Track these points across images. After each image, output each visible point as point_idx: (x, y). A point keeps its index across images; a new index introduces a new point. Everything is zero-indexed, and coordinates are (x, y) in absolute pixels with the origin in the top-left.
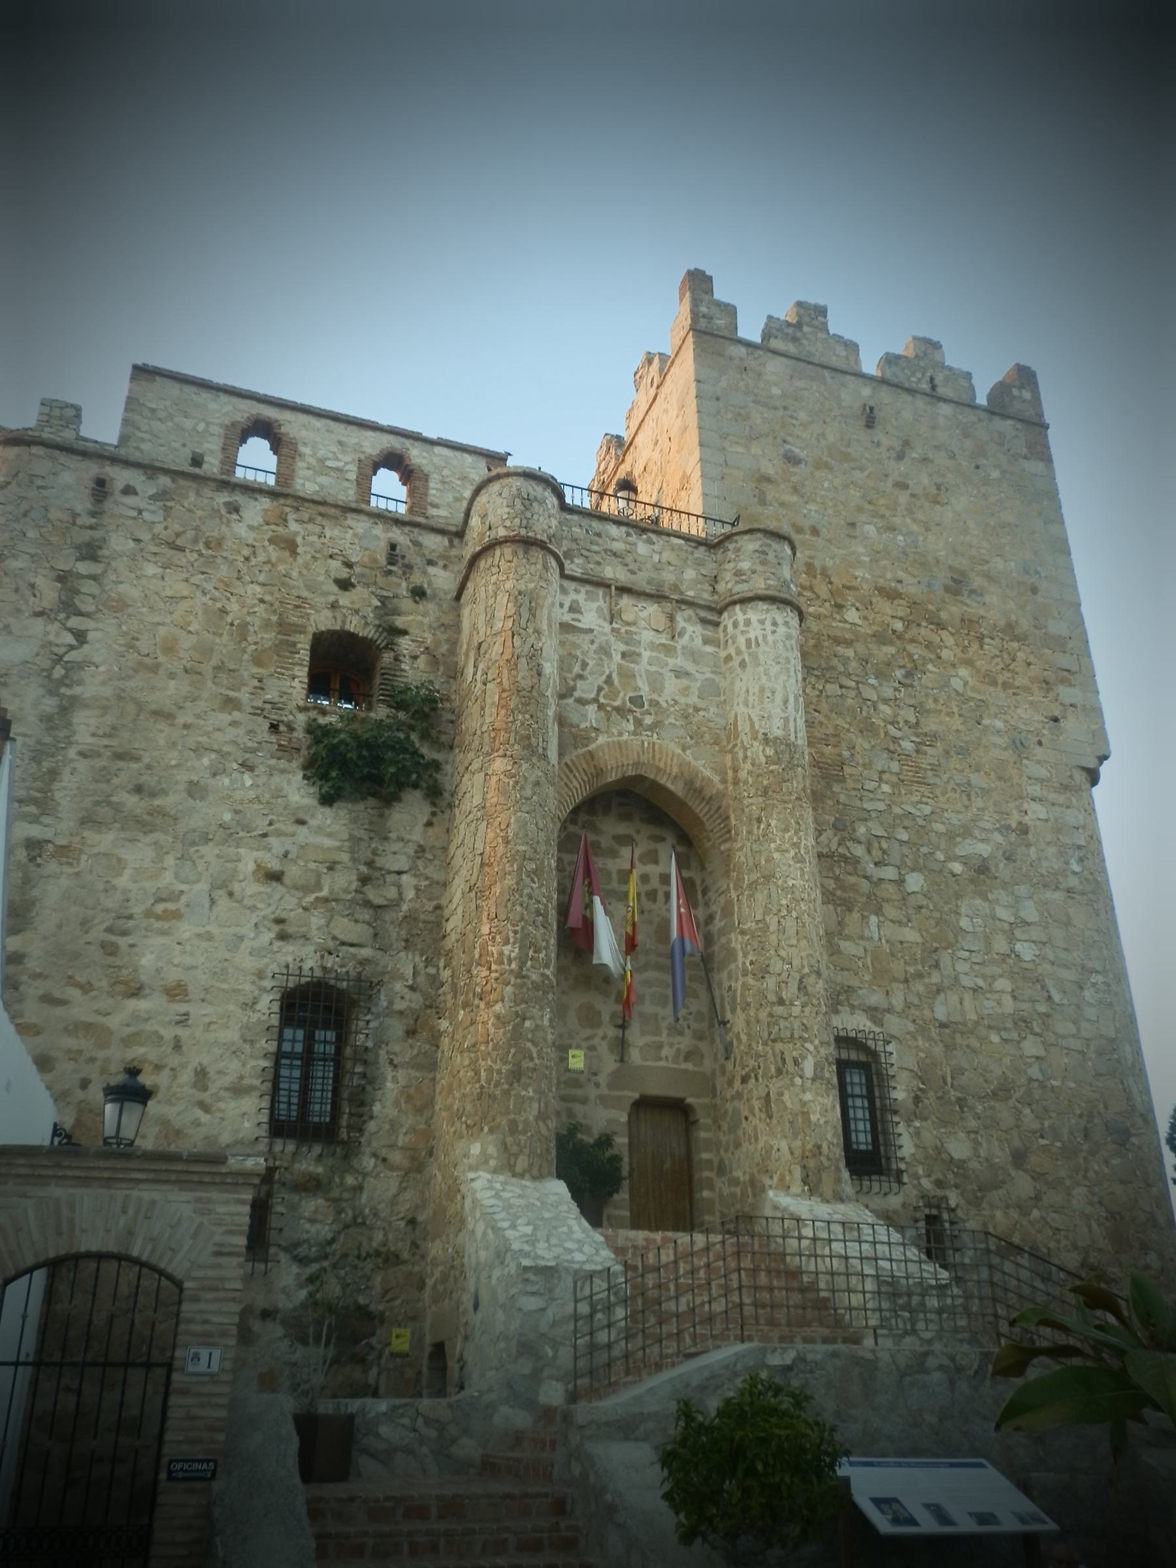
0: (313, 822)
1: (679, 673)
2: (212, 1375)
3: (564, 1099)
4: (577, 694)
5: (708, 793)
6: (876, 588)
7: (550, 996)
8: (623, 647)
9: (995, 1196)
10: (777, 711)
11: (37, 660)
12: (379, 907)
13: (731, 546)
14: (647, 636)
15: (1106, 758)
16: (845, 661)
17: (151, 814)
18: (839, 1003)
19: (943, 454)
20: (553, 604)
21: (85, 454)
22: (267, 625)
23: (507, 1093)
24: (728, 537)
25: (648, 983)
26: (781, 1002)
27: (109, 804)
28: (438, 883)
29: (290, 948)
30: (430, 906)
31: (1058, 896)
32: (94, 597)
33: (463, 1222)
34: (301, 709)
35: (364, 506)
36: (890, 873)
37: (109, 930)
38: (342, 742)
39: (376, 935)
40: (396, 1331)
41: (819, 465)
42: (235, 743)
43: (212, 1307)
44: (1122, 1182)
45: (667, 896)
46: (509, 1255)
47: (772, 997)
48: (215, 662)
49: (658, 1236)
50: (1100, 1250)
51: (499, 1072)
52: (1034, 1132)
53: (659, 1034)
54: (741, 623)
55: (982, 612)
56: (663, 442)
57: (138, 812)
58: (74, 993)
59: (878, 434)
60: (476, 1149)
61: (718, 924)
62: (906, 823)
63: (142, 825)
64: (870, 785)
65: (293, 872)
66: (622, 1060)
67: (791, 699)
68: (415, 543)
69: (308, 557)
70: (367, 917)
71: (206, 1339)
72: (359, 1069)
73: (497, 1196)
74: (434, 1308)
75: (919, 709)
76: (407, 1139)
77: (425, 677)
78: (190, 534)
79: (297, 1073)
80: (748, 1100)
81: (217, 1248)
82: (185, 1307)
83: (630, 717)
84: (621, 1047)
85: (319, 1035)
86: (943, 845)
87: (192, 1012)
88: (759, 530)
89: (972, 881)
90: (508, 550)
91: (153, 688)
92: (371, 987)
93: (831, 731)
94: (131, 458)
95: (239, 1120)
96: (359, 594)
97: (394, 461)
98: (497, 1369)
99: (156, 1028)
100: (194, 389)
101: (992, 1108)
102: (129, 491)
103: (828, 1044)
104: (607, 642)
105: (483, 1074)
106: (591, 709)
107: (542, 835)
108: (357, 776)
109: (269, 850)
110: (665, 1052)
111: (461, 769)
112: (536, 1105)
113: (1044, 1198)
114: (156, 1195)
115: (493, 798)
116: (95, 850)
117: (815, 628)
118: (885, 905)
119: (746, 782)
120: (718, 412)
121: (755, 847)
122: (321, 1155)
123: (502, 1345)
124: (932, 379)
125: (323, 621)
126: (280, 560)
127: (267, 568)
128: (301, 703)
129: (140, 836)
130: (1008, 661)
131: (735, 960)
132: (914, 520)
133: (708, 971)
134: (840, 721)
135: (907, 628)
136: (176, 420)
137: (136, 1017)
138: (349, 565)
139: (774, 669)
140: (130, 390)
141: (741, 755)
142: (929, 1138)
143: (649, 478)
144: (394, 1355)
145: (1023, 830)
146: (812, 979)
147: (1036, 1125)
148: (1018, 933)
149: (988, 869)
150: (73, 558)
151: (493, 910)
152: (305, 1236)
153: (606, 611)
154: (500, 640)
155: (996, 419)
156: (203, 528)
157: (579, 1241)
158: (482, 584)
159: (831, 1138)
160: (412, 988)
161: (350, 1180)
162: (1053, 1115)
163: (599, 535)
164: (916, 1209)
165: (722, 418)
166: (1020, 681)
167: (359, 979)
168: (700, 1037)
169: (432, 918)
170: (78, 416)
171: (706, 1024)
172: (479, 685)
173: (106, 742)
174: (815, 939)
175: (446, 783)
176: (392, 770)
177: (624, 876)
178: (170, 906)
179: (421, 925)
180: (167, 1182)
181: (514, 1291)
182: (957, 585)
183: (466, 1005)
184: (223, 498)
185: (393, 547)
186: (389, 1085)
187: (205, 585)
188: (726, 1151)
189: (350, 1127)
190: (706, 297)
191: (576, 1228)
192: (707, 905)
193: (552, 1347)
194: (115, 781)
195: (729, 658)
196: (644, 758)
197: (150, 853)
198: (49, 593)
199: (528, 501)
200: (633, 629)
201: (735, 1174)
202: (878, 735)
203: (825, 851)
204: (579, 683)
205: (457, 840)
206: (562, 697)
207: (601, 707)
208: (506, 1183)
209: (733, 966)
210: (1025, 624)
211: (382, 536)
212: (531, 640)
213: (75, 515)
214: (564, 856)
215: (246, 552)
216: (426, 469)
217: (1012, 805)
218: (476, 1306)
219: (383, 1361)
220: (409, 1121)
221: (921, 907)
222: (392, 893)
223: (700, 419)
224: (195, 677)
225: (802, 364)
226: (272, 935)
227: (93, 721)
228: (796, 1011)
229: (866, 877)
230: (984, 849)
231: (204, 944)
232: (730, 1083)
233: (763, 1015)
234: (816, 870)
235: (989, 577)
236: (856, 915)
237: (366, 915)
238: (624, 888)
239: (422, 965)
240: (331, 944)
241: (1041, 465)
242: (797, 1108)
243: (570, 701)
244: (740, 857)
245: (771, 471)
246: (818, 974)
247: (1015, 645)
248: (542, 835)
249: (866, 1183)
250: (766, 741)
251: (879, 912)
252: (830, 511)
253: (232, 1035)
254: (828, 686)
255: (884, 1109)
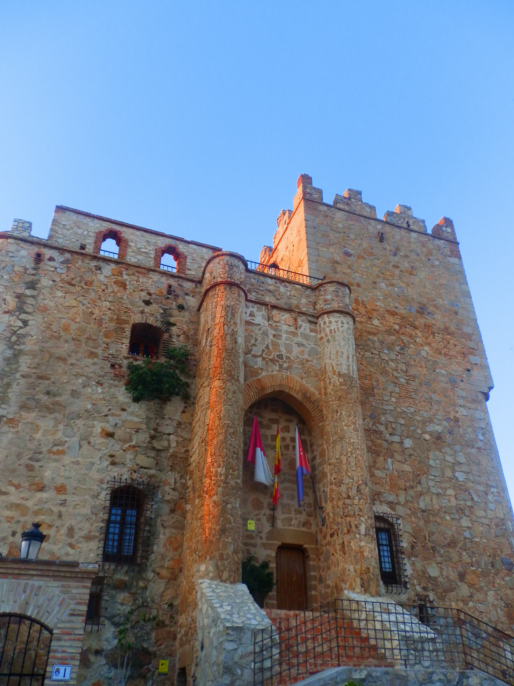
0: (129, 410)
1: (299, 345)
2: (66, 681)
3: (245, 544)
4: (253, 353)
5: (313, 399)
6: (386, 310)
7: (240, 493)
8: (274, 332)
9: (452, 595)
10: (344, 362)
11: (5, 333)
12: (159, 450)
13: (322, 289)
14: (285, 328)
15: (492, 388)
16: (373, 342)
17: (54, 405)
18: (374, 500)
19: (414, 254)
20: (242, 312)
21: (32, 243)
22: (111, 320)
23: (218, 540)
24: (321, 285)
25: (285, 489)
26: (349, 497)
27: (34, 399)
28: (187, 439)
29: (117, 469)
30: (183, 450)
31: (474, 451)
32: (33, 305)
33: (196, 605)
34: (126, 358)
35: (157, 269)
36: (396, 439)
37: (31, 459)
38: (144, 372)
39: (157, 463)
40: (161, 661)
41: (360, 257)
42: (94, 372)
43: (68, 643)
44: (511, 589)
45: (294, 447)
46: (219, 621)
47: (344, 495)
48: (86, 336)
49: (291, 613)
50: (502, 623)
51: (215, 529)
52: (468, 564)
53: (291, 514)
54: (327, 322)
55: (433, 322)
56: (290, 247)
57: (47, 403)
58: (12, 489)
59: (385, 245)
60: (203, 568)
61: (318, 461)
62: (403, 416)
63: (49, 410)
64: (386, 398)
65: (119, 433)
66: (273, 526)
67: (351, 357)
68: (180, 285)
69: (131, 290)
70: (153, 455)
71: (63, 662)
72: (147, 528)
73: (213, 591)
74: (181, 650)
75: (407, 364)
76: (170, 563)
77: (183, 344)
78: (78, 279)
79: (117, 531)
80: (334, 545)
81: (71, 612)
82: (53, 643)
83: (277, 364)
84: (273, 519)
85: (129, 512)
86: (420, 426)
87: (68, 499)
88: (335, 282)
89: (434, 443)
90: (222, 288)
91: (58, 347)
92: (154, 489)
93: (368, 373)
94: (53, 245)
95: (88, 554)
96: (154, 307)
97: (171, 250)
98: (212, 681)
99: (51, 506)
100: (83, 217)
101: (448, 551)
102: (51, 259)
103: (371, 518)
104: (266, 330)
105: (207, 530)
106: (259, 359)
107: (236, 416)
108: (151, 388)
109: (108, 422)
110: (294, 522)
111: (199, 386)
112: (232, 546)
113: (475, 596)
114: (41, 583)
115: (213, 398)
116: (26, 421)
117: (359, 328)
118: (395, 453)
119: (330, 394)
120: (315, 233)
121: (335, 424)
122: (127, 571)
123: (215, 668)
124: (408, 222)
125: (137, 319)
126: (118, 291)
127: (112, 294)
128: (126, 355)
129: (48, 415)
130: (446, 344)
131: (327, 477)
132: (402, 281)
133: (313, 483)
134: (371, 369)
135: (400, 328)
136: (74, 229)
137: (41, 501)
138: (149, 294)
139: (343, 343)
140: (54, 216)
141: (328, 381)
142: (419, 566)
143: (284, 263)
144: (160, 674)
145: (457, 420)
146: (363, 487)
147: (469, 560)
148: (456, 468)
149: (441, 438)
150: (24, 288)
151: (213, 451)
152: (118, 612)
153: (266, 316)
154: (218, 327)
155: (436, 240)
156: (84, 276)
157: (254, 614)
158: (209, 303)
159: (374, 564)
160: (174, 489)
161: (141, 584)
162: (477, 555)
163: (263, 283)
164: (414, 601)
165: (316, 236)
166: (451, 353)
167: (148, 484)
168: (309, 515)
169: (184, 456)
170: (30, 227)
171: (312, 509)
172: (208, 347)
173: (34, 371)
174: (364, 467)
175: (192, 393)
176: (167, 386)
177: (274, 438)
178: (60, 448)
179: (179, 459)
180: (48, 576)
181: (221, 639)
182: (422, 310)
183: (199, 496)
184: (94, 263)
185: (170, 287)
186: (161, 536)
187: (84, 301)
188: (323, 571)
189: (142, 557)
190: (310, 186)
191: (252, 607)
192: (312, 452)
193: (241, 669)
194: (38, 389)
195: (322, 338)
196: (284, 383)
197: (52, 423)
198: (12, 303)
199: (231, 266)
200: (278, 324)
201: (328, 582)
202: (389, 375)
203: (367, 428)
204: (254, 348)
205: (197, 419)
206: (246, 354)
207: (264, 359)
208: (217, 585)
209: (325, 481)
210: (453, 328)
211: (165, 282)
212: (232, 327)
213: (26, 269)
214: (246, 428)
215: (103, 287)
216: (186, 254)
217: (451, 409)
218: (202, 648)
219: (155, 677)
220: (171, 554)
221: (411, 455)
222: (165, 444)
223: (307, 236)
224: (77, 342)
225: (351, 215)
226: (108, 463)
227: (29, 361)
228: (356, 502)
229: (386, 441)
230: (439, 428)
231: (75, 467)
232: (325, 537)
233: (340, 504)
234: (363, 435)
235: (436, 307)
236: (381, 458)
237: (153, 454)
238: (274, 443)
239: (179, 478)
240: (136, 467)
241: (457, 260)
242: (358, 549)
243: (250, 356)
244: (328, 429)
245: (339, 259)
246: (366, 484)
247: (449, 337)
248: (236, 416)
249: (390, 588)
250: (340, 375)
251: (392, 457)
252: (365, 277)
253: (87, 511)
254: (366, 353)
255: (397, 551)
